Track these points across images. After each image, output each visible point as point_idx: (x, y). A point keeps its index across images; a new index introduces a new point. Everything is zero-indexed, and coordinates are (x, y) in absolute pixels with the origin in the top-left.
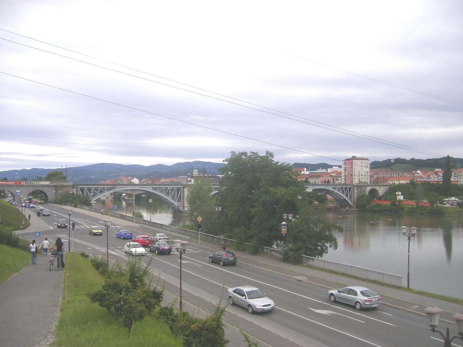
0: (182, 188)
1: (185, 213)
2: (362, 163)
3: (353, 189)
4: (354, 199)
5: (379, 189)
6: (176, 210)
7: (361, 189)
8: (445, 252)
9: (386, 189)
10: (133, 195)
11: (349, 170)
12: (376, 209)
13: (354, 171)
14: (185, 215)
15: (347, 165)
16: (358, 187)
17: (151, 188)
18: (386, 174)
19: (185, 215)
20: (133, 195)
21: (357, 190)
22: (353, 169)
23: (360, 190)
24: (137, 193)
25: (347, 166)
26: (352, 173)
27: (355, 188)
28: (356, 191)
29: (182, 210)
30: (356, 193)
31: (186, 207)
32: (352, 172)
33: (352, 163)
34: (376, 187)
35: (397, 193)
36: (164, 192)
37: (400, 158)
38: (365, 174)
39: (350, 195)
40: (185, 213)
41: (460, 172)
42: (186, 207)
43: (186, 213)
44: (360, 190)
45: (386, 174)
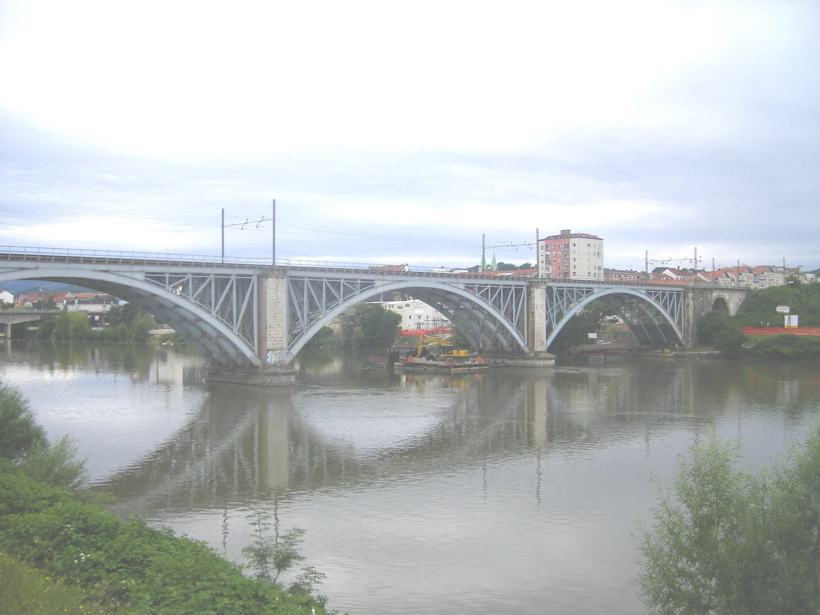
0: (255, 279)
1: (270, 374)
2: (589, 245)
3: (685, 297)
4: (687, 325)
5: (730, 297)
6: (223, 360)
7: (703, 297)
8: (26, 401)
9: (740, 299)
10: (6, 325)
11: (559, 261)
12: (786, 350)
13: (572, 263)
14: (269, 380)
15: (554, 250)
16: (697, 292)
17: (141, 276)
18: (617, 276)
19: (269, 380)
20: (6, 325)
21: (693, 298)
22: (568, 259)
23: (702, 301)
24: (17, 321)
25: (554, 253)
26: (565, 269)
27: (690, 295)
28: (691, 303)
29: (256, 361)
30: (693, 308)
31: (273, 350)
32: (568, 267)
33: (567, 246)
34: (724, 294)
35: (779, 309)
36: (191, 294)
37: (503, 263)
38: (595, 272)
39: (678, 314)
40: (270, 374)
41: (762, 273)
42: (273, 350)
43: (276, 374)
44: (701, 299)
45: (617, 276)
